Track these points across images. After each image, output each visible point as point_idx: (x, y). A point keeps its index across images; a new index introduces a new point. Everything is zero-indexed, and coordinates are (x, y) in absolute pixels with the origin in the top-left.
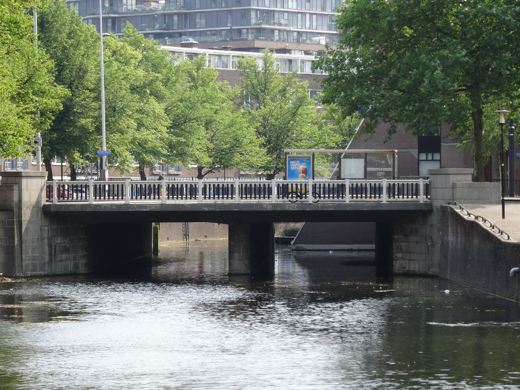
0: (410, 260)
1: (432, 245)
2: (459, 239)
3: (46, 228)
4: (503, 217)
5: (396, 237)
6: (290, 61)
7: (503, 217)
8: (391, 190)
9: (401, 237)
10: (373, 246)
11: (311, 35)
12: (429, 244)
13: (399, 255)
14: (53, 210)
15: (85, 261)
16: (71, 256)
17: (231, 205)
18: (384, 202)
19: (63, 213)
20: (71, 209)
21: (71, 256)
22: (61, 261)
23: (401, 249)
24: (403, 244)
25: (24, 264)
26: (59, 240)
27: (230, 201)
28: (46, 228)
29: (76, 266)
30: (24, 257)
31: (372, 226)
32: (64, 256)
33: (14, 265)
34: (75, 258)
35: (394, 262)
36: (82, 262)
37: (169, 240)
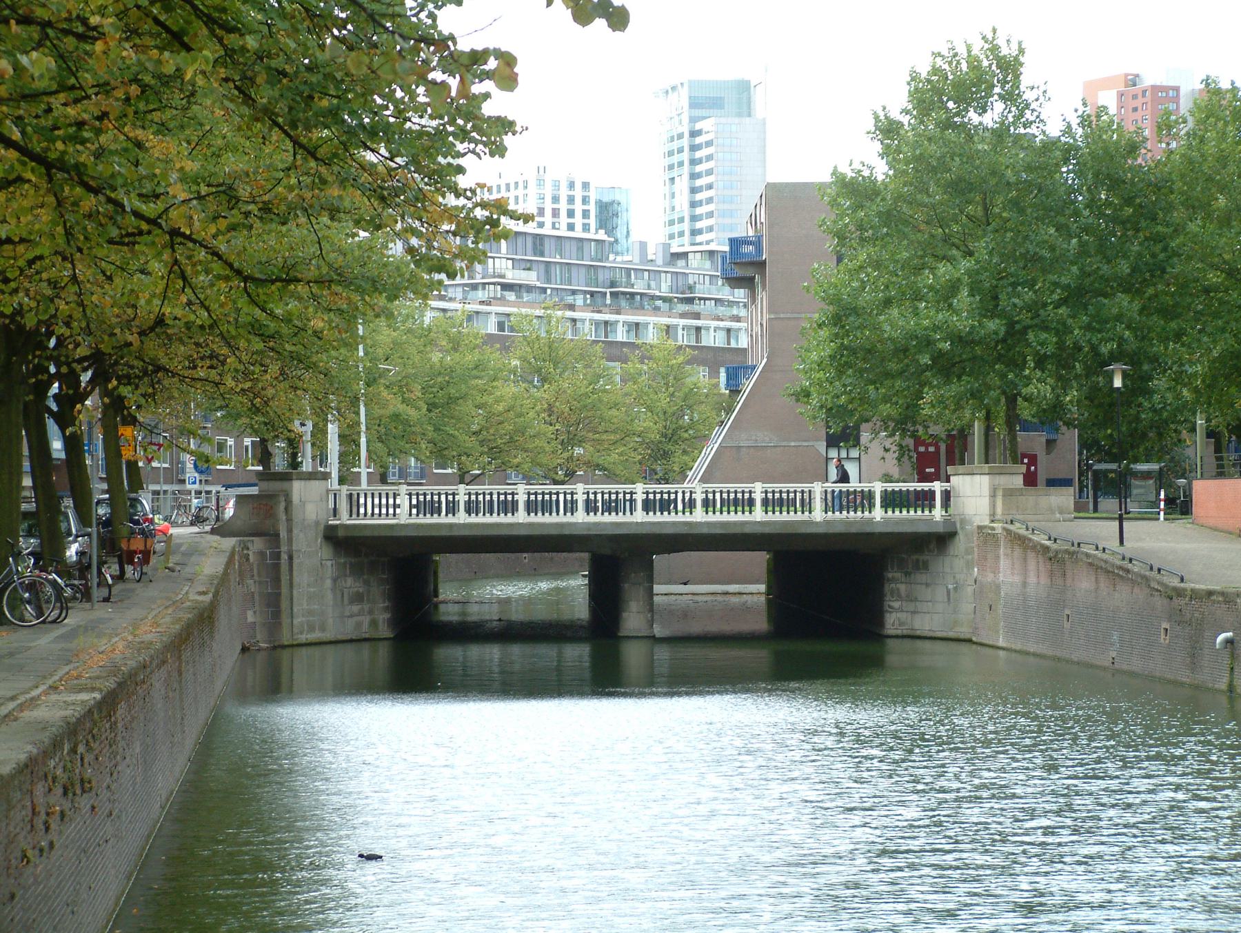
0: (914, 613)
1: (956, 589)
2: (1032, 579)
3: (329, 563)
4: (1122, 542)
5: (890, 575)
6: (574, 321)
7: (1122, 542)
8: (571, 507)
9: (898, 575)
10: (762, 588)
11: (564, 294)
12: (950, 587)
13: (896, 605)
14: (341, 533)
15: (387, 616)
16: (366, 607)
17: (451, 526)
18: (878, 519)
19: (354, 538)
20: (367, 533)
21: (366, 607)
22: (351, 616)
23: (899, 595)
24: (902, 587)
25: (295, 622)
26: (350, 581)
27: (746, 517)
28: (329, 563)
29: (374, 623)
30: (295, 610)
31: (761, 559)
32: (355, 608)
33: (280, 624)
34: (371, 612)
35: (887, 615)
36: (383, 617)
37: (746, 591)
